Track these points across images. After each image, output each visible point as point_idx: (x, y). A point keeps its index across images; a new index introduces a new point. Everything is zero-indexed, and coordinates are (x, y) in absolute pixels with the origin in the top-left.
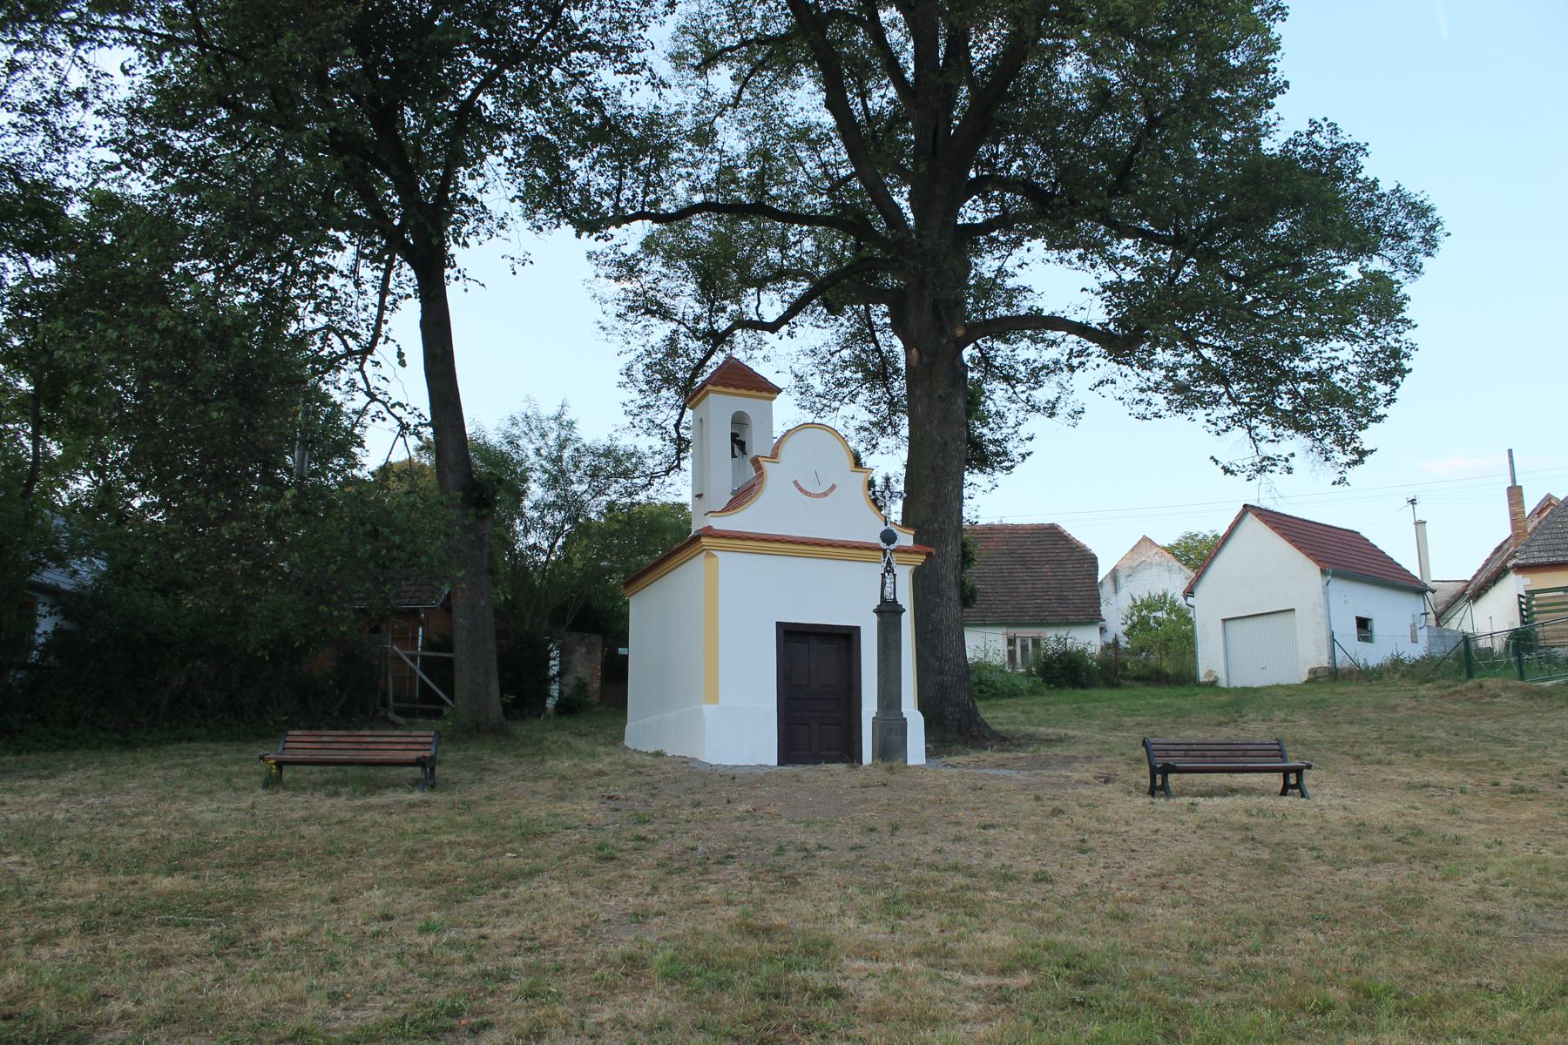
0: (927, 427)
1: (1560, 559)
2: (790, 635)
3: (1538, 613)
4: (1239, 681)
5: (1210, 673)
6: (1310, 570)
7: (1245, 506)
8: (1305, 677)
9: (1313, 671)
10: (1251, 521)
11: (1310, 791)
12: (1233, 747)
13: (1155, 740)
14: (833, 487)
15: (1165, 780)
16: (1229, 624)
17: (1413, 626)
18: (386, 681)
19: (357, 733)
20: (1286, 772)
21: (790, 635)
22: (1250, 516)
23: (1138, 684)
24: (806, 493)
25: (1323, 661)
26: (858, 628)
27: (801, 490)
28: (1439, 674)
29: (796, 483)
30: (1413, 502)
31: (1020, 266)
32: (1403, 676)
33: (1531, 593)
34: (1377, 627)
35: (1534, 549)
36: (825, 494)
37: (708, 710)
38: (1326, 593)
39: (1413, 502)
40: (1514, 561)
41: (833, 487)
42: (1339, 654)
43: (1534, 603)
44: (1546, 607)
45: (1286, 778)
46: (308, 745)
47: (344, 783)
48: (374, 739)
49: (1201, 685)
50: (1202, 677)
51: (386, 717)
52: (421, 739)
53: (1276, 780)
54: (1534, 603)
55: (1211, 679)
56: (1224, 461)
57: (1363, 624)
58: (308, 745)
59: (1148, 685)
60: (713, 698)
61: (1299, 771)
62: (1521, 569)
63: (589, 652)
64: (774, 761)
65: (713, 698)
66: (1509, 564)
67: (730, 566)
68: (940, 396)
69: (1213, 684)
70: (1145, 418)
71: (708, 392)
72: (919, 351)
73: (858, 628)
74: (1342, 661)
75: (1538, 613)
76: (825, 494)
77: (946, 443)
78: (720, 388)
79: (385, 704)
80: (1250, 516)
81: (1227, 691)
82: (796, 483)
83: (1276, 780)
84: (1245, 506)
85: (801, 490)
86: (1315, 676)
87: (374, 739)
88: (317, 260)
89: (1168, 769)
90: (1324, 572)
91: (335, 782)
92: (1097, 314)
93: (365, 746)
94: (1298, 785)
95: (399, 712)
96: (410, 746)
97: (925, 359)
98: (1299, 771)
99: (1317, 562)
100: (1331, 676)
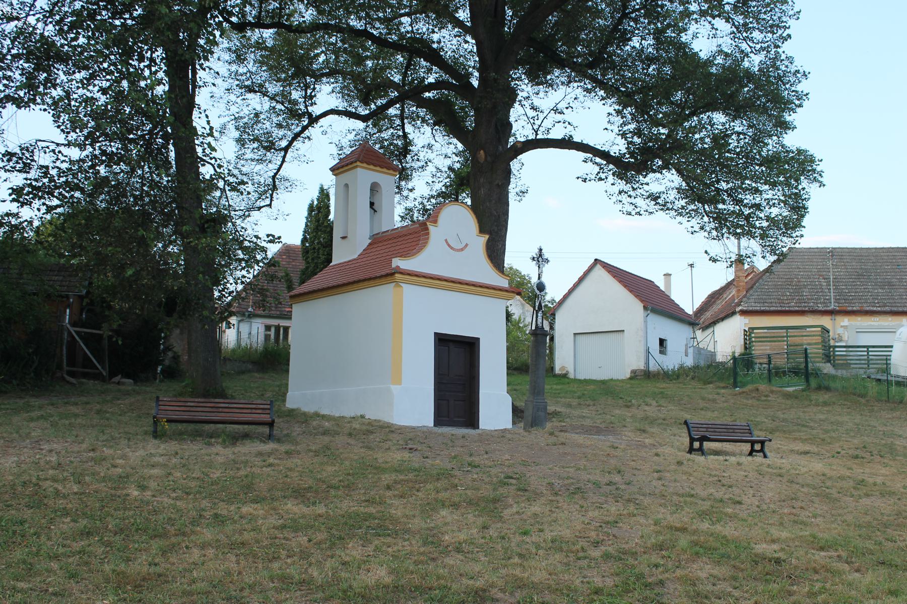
0: (488, 204)
1: (768, 309)
2: (442, 341)
3: (755, 342)
4: (581, 377)
5: (563, 368)
6: (637, 306)
7: (596, 260)
8: (628, 376)
9: (634, 372)
10: (599, 271)
11: (768, 454)
12: (728, 427)
13: (690, 421)
14: (467, 245)
15: (701, 445)
16: (578, 337)
17: (686, 345)
18: (62, 350)
19: (212, 400)
20: (753, 443)
21: (442, 341)
22: (598, 266)
23: (515, 373)
24: (452, 248)
25: (641, 366)
26: (478, 339)
27: (449, 245)
28: (715, 379)
29: (446, 241)
30: (691, 266)
31: (567, 108)
32: (693, 378)
33: (752, 329)
34: (670, 345)
35: (752, 300)
36: (462, 250)
37: (395, 388)
38: (646, 322)
39: (691, 266)
40: (740, 308)
41: (467, 245)
42: (652, 362)
43: (753, 335)
44: (762, 339)
45: (752, 446)
46: (178, 408)
47: (181, 434)
48: (227, 405)
49: (555, 376)
50: (557, 370)
51: (63, 379)
52: (262, 406)
53: (747, 447)
54: (753, 335)
55: (564, 372)
56: (713, 254)
57: (662, 342)
58: (178, 408)
59: (521, 373)
60: (399, 383)
61: (762, 443)
62: (744, 313)
63: (181, 333)
64: (432, 424)
65: (399, 383)
66: (738, 309)
67: (410, 292)
68: (498, 185)
69: (565, 376)
70: (630, 214)
71: (356, 167)
72: (485, 152)
73: (478, 339)
74: (653, 367)
75: (755, 342)
76: (462, 250)
77: (499, 216)
78: (365, 165)
79: (60, 367)
80: (598, 266)
81: (576, 381)
82: (446, 241)
83: (747, 447)
84: (596, 260)
85: (449, 245)
86: (635, 375)
87: (227, 405)
88: (721, 206)
89: (703, 439)
90: (645, 308)
91: (181, 434)
92: (618, 147)
93: (221, 410)
94: (762, 450)
95: (72, 374)
96: (254, 411)
97: (489, 159)
98: (762, 443)
99: (642, 301)
100: (645, 376)
